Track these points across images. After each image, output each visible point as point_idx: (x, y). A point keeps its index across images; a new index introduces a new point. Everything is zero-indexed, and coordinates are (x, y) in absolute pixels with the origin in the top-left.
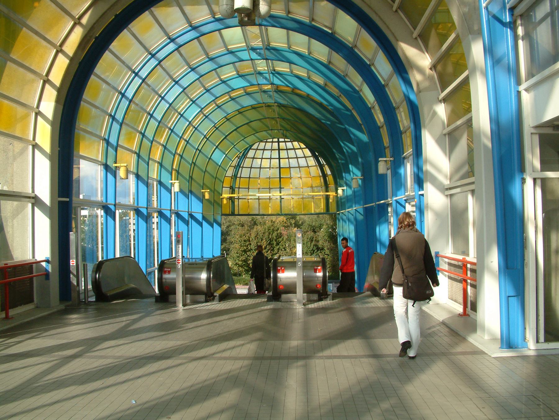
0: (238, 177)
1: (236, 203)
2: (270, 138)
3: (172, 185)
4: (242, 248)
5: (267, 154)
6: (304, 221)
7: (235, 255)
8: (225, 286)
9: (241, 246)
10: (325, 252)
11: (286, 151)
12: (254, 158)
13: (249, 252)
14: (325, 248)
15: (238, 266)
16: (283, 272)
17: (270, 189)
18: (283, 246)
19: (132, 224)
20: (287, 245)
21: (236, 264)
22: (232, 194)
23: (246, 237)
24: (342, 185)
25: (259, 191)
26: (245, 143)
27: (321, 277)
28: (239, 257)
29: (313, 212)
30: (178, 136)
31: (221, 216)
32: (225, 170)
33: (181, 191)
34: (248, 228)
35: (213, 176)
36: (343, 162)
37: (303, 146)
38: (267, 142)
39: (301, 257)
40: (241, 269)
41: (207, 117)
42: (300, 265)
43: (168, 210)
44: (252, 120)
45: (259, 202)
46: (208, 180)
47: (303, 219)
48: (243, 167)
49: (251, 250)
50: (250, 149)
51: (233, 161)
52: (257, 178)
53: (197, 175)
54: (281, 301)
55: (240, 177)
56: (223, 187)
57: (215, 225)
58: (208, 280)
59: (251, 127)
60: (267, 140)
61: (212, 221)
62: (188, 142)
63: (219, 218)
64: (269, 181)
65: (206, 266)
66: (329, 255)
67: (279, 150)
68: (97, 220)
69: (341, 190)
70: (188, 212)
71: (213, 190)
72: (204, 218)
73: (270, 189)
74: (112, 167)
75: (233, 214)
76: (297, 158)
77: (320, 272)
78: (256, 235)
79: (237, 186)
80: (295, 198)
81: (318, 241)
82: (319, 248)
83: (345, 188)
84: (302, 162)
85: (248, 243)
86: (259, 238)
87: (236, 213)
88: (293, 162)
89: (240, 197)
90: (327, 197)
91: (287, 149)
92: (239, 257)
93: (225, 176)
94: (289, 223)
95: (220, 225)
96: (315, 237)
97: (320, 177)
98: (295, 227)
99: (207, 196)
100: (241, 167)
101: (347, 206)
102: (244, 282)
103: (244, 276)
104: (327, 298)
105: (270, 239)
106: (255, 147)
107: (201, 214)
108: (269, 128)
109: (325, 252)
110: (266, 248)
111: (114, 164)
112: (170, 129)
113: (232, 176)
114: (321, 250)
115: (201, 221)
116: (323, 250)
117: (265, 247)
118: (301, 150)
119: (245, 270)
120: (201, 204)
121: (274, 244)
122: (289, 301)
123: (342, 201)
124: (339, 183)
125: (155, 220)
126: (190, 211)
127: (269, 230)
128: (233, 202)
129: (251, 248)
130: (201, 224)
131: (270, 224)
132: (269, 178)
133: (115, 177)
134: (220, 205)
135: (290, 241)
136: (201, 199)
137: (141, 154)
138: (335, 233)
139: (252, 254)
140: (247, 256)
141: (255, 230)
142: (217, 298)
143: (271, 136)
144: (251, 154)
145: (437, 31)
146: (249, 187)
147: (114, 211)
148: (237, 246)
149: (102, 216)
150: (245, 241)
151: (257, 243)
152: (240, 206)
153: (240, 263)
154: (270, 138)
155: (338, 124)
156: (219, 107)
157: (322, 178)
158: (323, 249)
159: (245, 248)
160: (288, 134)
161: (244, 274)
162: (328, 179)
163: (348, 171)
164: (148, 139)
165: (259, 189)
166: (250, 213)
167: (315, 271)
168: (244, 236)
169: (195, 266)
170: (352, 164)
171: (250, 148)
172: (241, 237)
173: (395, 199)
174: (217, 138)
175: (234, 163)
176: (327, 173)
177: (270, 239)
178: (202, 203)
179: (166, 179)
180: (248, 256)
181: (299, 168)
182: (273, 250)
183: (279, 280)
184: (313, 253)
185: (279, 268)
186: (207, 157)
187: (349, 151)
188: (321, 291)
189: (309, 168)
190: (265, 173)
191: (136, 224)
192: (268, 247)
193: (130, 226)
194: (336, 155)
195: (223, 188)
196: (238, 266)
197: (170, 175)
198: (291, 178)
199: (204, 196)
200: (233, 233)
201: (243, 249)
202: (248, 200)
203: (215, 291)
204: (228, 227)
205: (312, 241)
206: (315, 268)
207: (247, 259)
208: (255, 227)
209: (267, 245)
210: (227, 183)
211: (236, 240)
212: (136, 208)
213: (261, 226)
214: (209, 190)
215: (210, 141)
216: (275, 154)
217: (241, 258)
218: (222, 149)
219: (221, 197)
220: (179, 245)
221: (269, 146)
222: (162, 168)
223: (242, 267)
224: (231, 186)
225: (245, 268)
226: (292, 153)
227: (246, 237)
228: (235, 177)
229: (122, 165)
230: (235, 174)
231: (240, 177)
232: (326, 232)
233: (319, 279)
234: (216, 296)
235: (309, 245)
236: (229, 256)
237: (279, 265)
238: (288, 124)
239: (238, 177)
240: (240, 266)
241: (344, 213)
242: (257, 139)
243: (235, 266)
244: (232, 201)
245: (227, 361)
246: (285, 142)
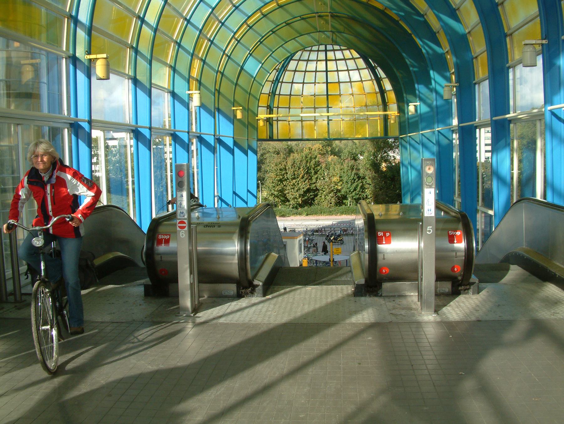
2: (317, 44)
3: (190, 97)
4: (278, 177)
5: (312, 66)
6: (340, 148)
7: (271, 185)
8: (274, 255)
9: (277, 175)
10: (366, 182)
11: (335, 62)
12: (295, 71)
13: (286, 182)
14: (367, 177)
15: (273, 196)
16: (388, 242)
17: (315, 108)
18: (321, 174)
19: (168, 153)
20: (326, 174)
21: (272, 194)
22: (270, 114)
23: (281, 165)
24: (409, 101)
25: (302, 111)
26: (285, 51)
27: (462, 251)
28: (274, 187)
29: (367, 136)
30: (197, 28)
31: (257, 141)
32: (261, 84)
33: (202, 106)
34: (284, 156)
35: (246, 92)
36: (415, 69)
37: (356, 55)
38: (311, 51)
39: (433, 215)
40: (277, 199)
41: (237, 8)
42: (429, 231)
43: (185, 132)
44: (296, 16)
45: (302, 124)
46: (240, 96)
47: (339, 146)
48: (282, 82)
49: (288, 179)
50: (291, 59)
51: (270, 74)
52: (300, 95)
53: (226, 88)
54: (381, 296)
55: (279, 95)
56: (258, 106)
57: (250, 152)
58: (243, 256)
59: (293, 28)
60: (312, 47)
61: (246, 147)
62: (212, 42)
63: (254, 144)
64: (315, 100)
65: (238, 231)
66: (370, 185)
67: (326, 60)
68: (126, 150)
69: (413, 107)
70: (214, 136)
71: (247, 108)
72: (235, 143)
73: (315, 108)
74: (83, 61)
75: (271, 139)
76: (348, 70)
77: (459, 241)
78: (293, 163)
79: (276, 105)
80: (347, 118)
81: (359, 170)
82: (360, 177)
83: (418, 104)
84: (355, 76)
85: (284, 172)
86: (296, 166)
87: (275, 137)
88: (343, 76)
89: (279, 119)
90: (386, 118)
91: (336, 60)
92: (274, 187)
93: (261, 93)
94: (325, 151)
95: (255, 152)
96: (355, 165)
97: (376, 93)
98: (331, 155)
99: (239, 115)
100: (280, 82)
101: (420, 126)
102: (280, 213)
103: (280, 207)
104: (468, 289)
105: (308, 168)
106: (297, 56)
107: (232, 138)
108: (317, 29)
109: (366, 182)
110: (304, 177)
111: (86, 56)
112: (186, 19)
113: (270, 93)
114: (362, 179)
115: (232, 147)
116: (364, 179)
117: (302, 176)
118: (353, 61)
119: (282, 200)
120: (232, 126)
121: (312, 173)
122: (396, 294)
123: (410, 121)
124: (405, 99)
125: (193, 148)
126: (218, 133)
127: (306, 157)
128: (271, 125)
129: (287, 177)
130: (232, 152)
131: (307, 151)
132: (314, 95)
133: (89, 77)
134: (256, 128)
135: (329, 170)
136: (232, 119)
137: (139, 49)
138: (377, 161)
139: (288, 184)
140: (283, 185)
141: (292, 157)
142: (259, 289)
143: (318, 42)
144: (292, 65)
146: (289, 106)
147: (89, 131)
148: (273, 175)
149: (131, 146)
150: (281, 170)
151: (294, 171)
152: (280, 129)
153: (276, 193)
154: (317, 44)
155: (414, 15)
156: (251, 28)
157: (379, 95)
158: (364, 178)
159: (281, 177)
160: (338, 40)
161: (280, 205)
162: (387, 96)
163: (427, 81)
164: (148, 25)
165: (302, 108)
166: (291, 138)
167: (451, 241)
168: (280, 165)
169: (216, 229)
170: (433, 70)
171: (290, 58)
172: (276, 165)
173: (549, 108)
174: (251, 40)
175: (272, 77)
176: (385, 89)
177: (308, 168)
178: (233, 125)
179: (181, 88)
180: (284, 186)
181: (351, 83)
182: (311, 179)
183: (380, 257)
184: (354, 182)
185: (380, 234)
186: (239, 65)
187: (430, 51)
188: (460, 278)
189: (362, 82)
190: (309, 90)
191: (173, 153)
192: (306, 177)
193: (165, 155)
194: (407, 60)
195: (259, 108)
196: (273, 196)
197: (213, 119)
198: (340, 95)
199: (235, 116)
200: (268, 161)
201: (279, 179)
202: (289, 121)
203: (255, 276)
204: (262, 155)
205: (353, 169)
206: (451, 233)
207: (283, 189)
208: (292, 154)
209: (304, 174)
210: (264, 101)
211: (271, 168)
212: (134, 128)
213: (298, 154)
214: (241, 108)
215: (241, 44)
217: (277, 189)
218: (257, 57)
219: (257, 118)
220: (182, 191)
221: (313, 56)
222: (176, 75)
223: (278, 197)
224: (268, 105)
225: (281, 198)
226: (342, 65)
227: (281, 165)
228: (273, 94)
229: (99, 56)
230: (272, 91)
232: (368, 160)
233: (458, 254)
234: (257, 286)
235: (350, 174)
236: (264, 186)
237: (378, 227)
238: (341, 25)
239: (277, 95)
240: (275, 196)
241: (412, 137)
242: (300, 46)
243: (271, 196)
244: (270, 123)
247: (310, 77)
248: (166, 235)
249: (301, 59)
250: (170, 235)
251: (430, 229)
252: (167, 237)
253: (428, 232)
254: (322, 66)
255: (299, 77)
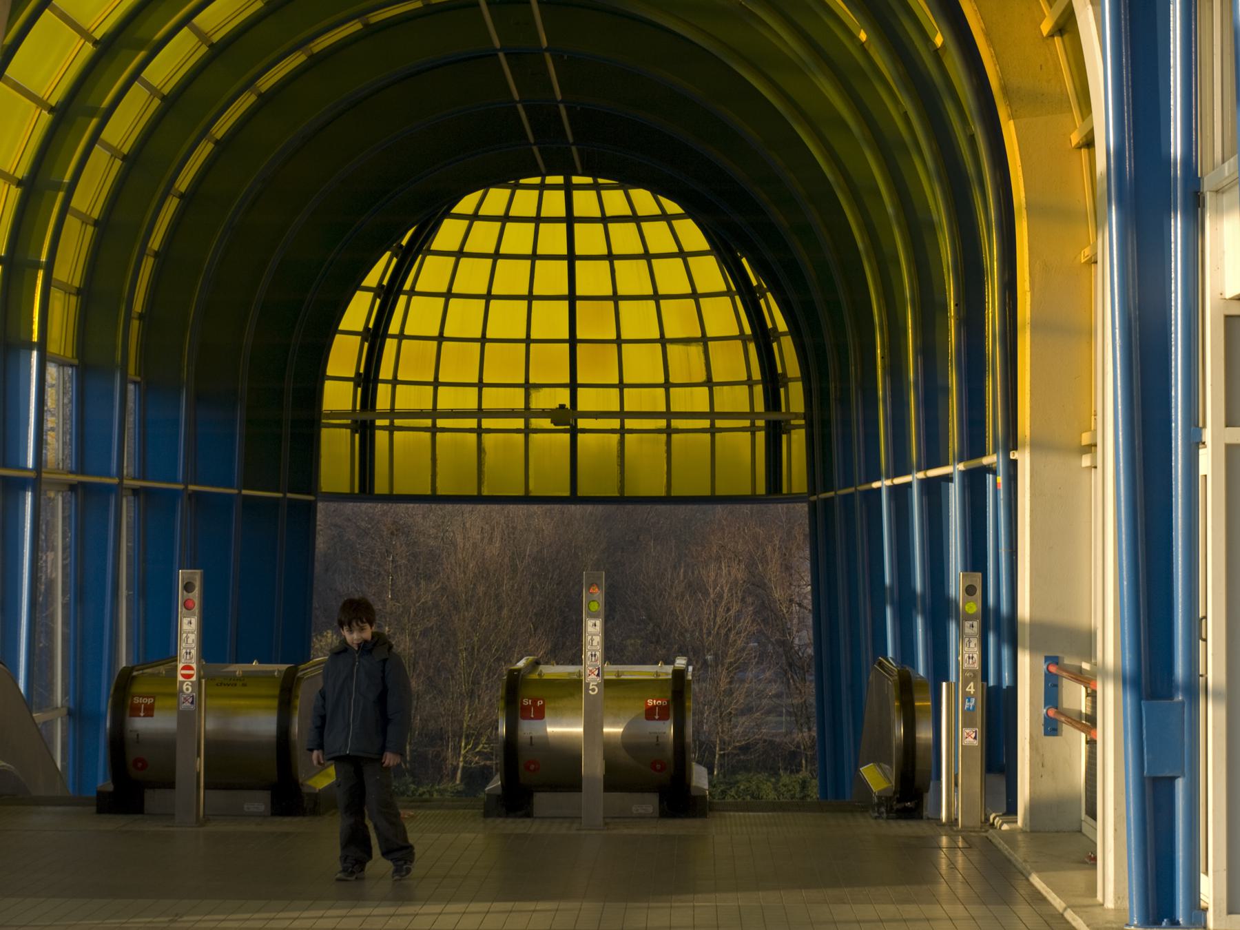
0: (393, 336)
1: (381, 437)
5: (518, 238)
12: (460, 254)
42: (593, 690)
48: (412, 292)
55: (401, 336)
84: (671, 276)
91: (605, 220)
100: (406, 293)
118: (664, 224)
145: (905, 666)
216: (553, 239)
221: (525, 202)
226: (625, 238)
231: (401, 336)
239: (393, 336)
245: (517, 903)
246: (597, 187)
247: (512, 277)
248: (148, 697)
249: (466, 250)
250: (154, 697)
251: (594, 687)
252: (150, 701)
253: (590, 692)
254: (553, 239)
255: (473, 276)
